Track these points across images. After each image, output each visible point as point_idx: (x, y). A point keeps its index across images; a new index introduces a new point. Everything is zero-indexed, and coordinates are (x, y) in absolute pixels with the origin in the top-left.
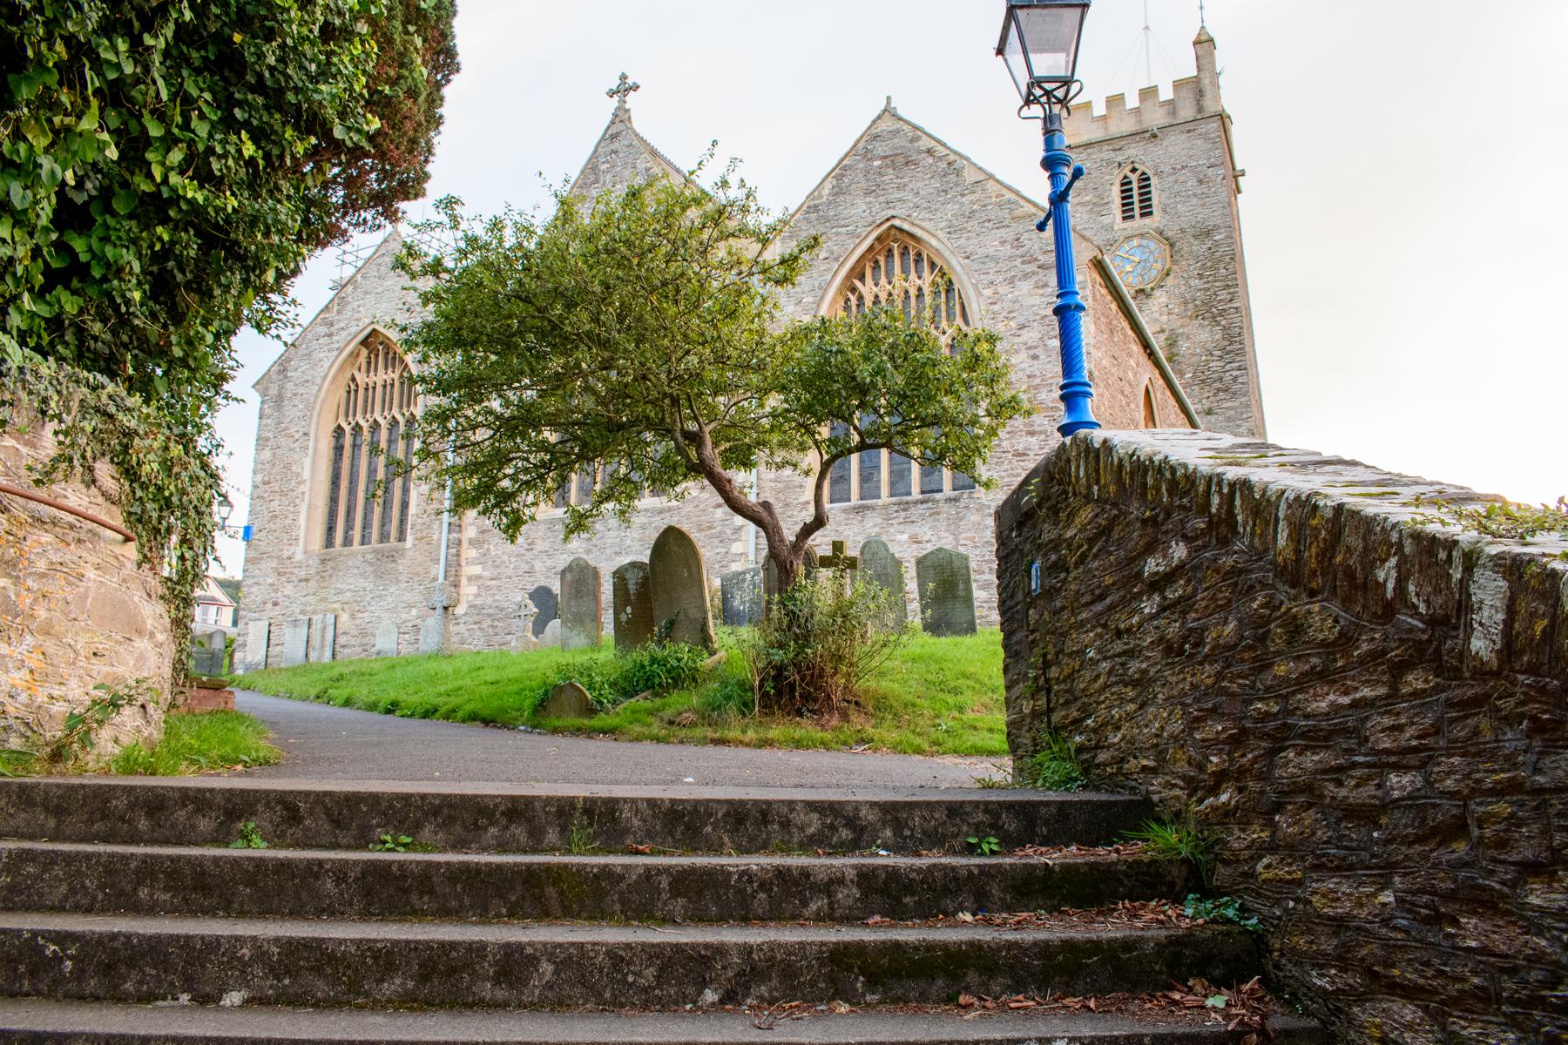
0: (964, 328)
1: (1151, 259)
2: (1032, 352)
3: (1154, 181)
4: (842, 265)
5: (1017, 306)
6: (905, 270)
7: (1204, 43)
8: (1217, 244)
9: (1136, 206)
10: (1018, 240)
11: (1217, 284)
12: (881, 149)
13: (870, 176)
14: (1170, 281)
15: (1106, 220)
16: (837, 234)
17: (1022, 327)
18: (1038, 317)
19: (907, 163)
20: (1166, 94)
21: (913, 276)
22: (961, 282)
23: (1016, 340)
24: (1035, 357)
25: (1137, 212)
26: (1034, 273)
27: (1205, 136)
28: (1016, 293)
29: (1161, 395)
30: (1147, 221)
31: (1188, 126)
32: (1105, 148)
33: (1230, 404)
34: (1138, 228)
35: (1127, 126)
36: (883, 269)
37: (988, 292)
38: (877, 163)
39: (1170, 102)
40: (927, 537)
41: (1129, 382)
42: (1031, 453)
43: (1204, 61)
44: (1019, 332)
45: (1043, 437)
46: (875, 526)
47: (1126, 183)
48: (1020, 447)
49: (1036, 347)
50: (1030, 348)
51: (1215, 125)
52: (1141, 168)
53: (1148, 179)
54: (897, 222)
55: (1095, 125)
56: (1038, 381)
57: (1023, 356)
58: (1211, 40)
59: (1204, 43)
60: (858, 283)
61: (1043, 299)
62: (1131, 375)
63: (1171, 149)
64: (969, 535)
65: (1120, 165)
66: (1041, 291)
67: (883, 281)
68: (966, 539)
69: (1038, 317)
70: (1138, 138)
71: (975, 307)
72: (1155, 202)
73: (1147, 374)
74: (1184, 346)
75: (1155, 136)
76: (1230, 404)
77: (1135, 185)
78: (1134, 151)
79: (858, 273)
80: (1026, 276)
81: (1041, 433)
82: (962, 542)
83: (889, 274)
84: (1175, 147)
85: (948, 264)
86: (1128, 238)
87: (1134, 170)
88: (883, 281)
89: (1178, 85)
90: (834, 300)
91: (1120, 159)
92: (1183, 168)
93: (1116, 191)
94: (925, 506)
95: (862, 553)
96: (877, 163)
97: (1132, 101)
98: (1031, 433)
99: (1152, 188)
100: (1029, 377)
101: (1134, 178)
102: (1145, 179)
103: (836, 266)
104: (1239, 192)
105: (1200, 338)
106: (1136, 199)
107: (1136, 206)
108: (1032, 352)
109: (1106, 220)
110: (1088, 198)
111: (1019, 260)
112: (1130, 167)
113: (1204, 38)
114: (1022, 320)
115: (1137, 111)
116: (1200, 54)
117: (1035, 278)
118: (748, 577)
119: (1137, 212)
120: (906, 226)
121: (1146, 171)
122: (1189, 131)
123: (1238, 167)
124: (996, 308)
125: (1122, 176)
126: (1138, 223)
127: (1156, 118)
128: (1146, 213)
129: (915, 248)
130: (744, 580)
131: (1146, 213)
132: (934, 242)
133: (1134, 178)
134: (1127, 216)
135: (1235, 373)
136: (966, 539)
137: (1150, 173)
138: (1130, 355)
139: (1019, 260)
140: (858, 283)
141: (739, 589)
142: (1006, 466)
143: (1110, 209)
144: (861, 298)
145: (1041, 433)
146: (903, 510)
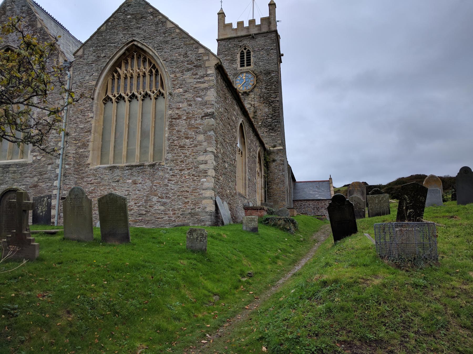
0: (162, 91)
1: (249, 81)
2: (189, 103)
3: (252, 53)
4: (111, 60)
5: (184, 82)
6: (139, 66)
7: (272, 6)
8: (272, 77)
9: (245, 62)
10: (186, 54)
11: (271, 91)
12: (131, 10)
13: (126, 22)
14: (256, 90)
15: (234, 66)
16: (109, 46)
17: (186, 92)
18: (192, 88)
19: (142, 18)
20: (258, 22)
21: (142, 67)
22: (161, 71)
23: (183, 97)
24: (190, 105)
25: (245, 64)
26: (191, 69)
27: (270, 38)
28: (184, 77)
29: (246, 128)
30: (249, 67)
31: (265, 35)
32: (236, 40)
33: (273, 134)
34: (245, 70)
35: (243, 33)
36: (129, 63)
37: (172, 76)
38: (128, 17)
39: (259, 26)
40: (140, 181)
41: (233, 120)
42: (187, 147)
43: (272, 12)
44: (184, 94)
45: (192, 140)
46: (118, 176)
47: (242, 53)
48: (182, 144)
49: (191, 101)
50: (188, 101)
51: (274, 35)
52: (248, 48)
53: (250, 52)
54: (136, 43)
55: (232, 32)
56: (191, 115)
57: (185, 104)
58: (275, 4)
59: (272, 6)
60: (119, 69)
61: (195, 80)
62: (234, 118)
63: (258, 42)
64: (158, 181)
65: (240, 46)
66: (194, 77)
67: (129, 68)
68: (157, 183)
69: (192, 88)
70: (247, 38)
71: (166, 81)
72: (252, 61)
73: (241, 120)
74: (259, 113)
75: (253, 37)
76: (273, 134)
77: (245, 54)
78: (246, 42)
79: (118, 64)
80: (188, 70)
81: (191, 138)
82: (154, 184)
83: (132, 66)
84: (260, 41)
85: (157, 62)
86: (242, 73)
87: (245, 49)
88: (129, 68)
89: (262, 20)
90: (107, 75)
91: (241, 44)
92: (262, 49)
93: (239, 56)
94: (140, 168)
95: (70, 194)
96: (128, 17)
97: (246, 24)
98: (187, 138)
99: (251, 56)
100: (187, 113)
101: (245, 51)
102: (249, 53)
103: (108, 60)
104: (281, 62)
105: (265, 110)
106: (245, 59)
107: (245, 62)
108: (189, 103)
109: (234, 66)
110: (229, 58)
111: (186, 63)
112: (244, 48)
113: (272, 3)
114: (185, 89)
115: (247, 28)
116: (270, 9)
117: (192, 71)
118: (45, 199)
119: (245, 64)
120: (139, 45)
121: (249, 49)
122: (265, 36)
123: (281, 53)
124: (175, 83)
125: (241, 50)
126: (246, 68)
127: (254, 31)
128: (249, 65)
129: (143, 55)
130: (44, 200)
131: (249, 65)
132: (151, 53)
133: (245, 51)
134: (242, 65)
135: (276, 123)
136: (157, 183)
137: (251, 50)
138: (234, 110)
139: (186, 63)
140: (119, 69)
141: (41, 205)
142: (175, 151)
143: (236, 63)
144: (119, 76)
145: (191, 138)
146: (130, 169)
